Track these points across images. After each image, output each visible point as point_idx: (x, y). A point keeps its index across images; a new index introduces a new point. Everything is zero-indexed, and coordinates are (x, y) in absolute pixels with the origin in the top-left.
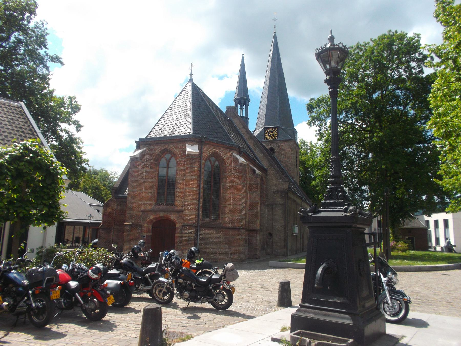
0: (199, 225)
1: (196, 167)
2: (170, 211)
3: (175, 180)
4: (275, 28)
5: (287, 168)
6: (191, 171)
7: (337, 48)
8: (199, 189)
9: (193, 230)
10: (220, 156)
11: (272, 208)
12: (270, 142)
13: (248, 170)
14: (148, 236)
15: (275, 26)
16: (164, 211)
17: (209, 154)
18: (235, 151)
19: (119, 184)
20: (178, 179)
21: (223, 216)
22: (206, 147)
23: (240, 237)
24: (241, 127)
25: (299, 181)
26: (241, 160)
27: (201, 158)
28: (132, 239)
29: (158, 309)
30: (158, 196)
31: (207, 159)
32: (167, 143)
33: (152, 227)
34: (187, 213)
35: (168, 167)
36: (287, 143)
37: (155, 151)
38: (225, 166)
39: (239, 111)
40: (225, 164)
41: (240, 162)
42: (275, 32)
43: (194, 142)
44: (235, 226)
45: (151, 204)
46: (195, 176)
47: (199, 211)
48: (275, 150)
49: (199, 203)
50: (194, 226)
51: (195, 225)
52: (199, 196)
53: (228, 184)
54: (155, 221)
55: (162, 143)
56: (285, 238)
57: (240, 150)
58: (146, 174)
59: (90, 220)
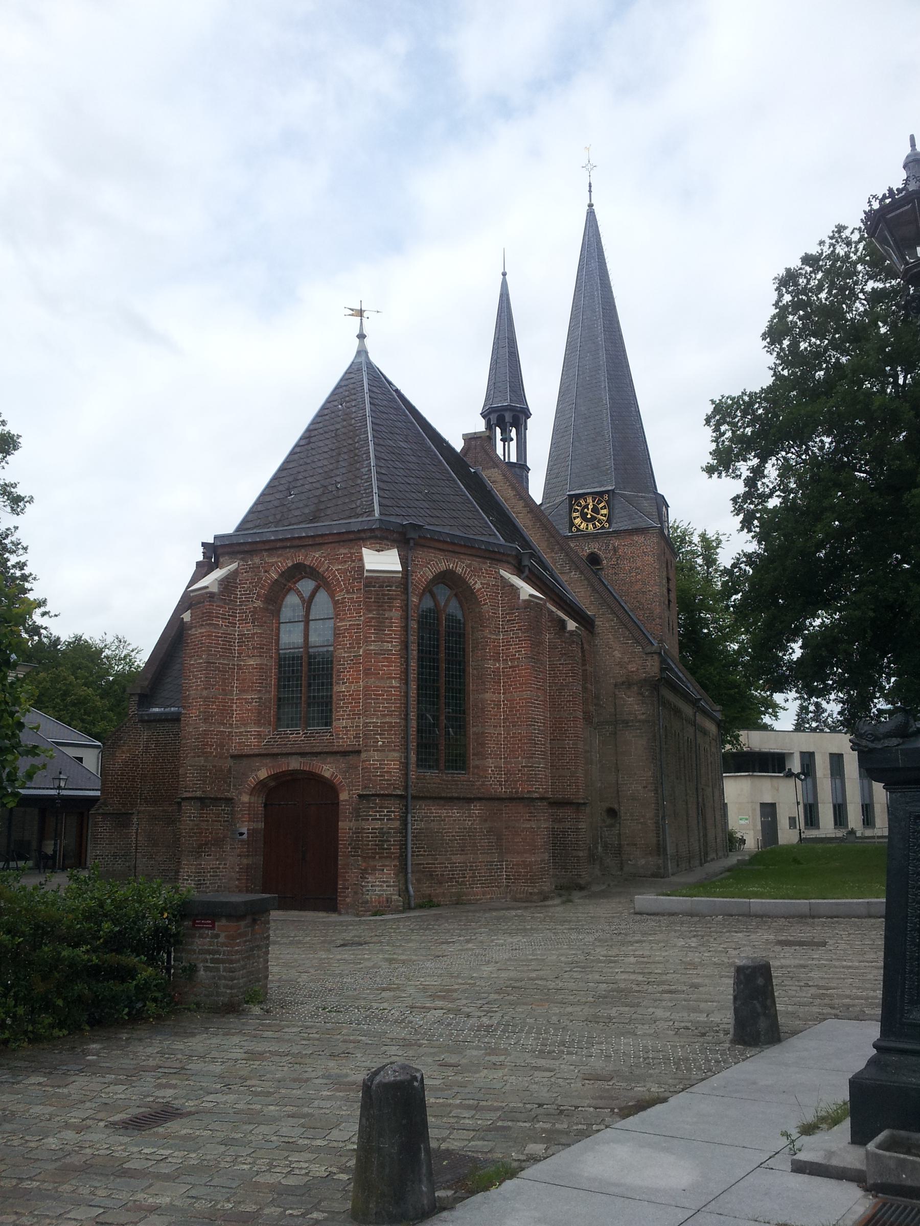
1: (395, 615)
2: (320, 753)
3: (332, 656)
4: (590, 191)
5: (641, 613)
6: (380, 629)
8: (407, 684)
9: (395, 809)
12: (587, 536)
14: (251, 833)
15: (590, 186)
16: (303, 754)
19: (150, 676)
21: (477, 763)
22: (421, 555)
24: (511, 493)
25: (677, 650)
26: (527, 590)
27: (406, 589)
28: (206, 844)
29: (416, 1084)
30: (279, 707)
31: (424, 591)
33: (266, 805)
34: (373, 758)
35: (307, 621)
37: (266, 572)
38: (477, 610)
39: (499, 445)
41: (524, 596)
43: (385, 542)
44: (517, 792)
45: (259, 735)
47: (407, 749)
49: (406, 726)
50: (397, 796)
52: (407, 707)
53: (490, 665)
54: (273, 784)
56: (657, 823)
57: (520, 562)
59: (59, 788)
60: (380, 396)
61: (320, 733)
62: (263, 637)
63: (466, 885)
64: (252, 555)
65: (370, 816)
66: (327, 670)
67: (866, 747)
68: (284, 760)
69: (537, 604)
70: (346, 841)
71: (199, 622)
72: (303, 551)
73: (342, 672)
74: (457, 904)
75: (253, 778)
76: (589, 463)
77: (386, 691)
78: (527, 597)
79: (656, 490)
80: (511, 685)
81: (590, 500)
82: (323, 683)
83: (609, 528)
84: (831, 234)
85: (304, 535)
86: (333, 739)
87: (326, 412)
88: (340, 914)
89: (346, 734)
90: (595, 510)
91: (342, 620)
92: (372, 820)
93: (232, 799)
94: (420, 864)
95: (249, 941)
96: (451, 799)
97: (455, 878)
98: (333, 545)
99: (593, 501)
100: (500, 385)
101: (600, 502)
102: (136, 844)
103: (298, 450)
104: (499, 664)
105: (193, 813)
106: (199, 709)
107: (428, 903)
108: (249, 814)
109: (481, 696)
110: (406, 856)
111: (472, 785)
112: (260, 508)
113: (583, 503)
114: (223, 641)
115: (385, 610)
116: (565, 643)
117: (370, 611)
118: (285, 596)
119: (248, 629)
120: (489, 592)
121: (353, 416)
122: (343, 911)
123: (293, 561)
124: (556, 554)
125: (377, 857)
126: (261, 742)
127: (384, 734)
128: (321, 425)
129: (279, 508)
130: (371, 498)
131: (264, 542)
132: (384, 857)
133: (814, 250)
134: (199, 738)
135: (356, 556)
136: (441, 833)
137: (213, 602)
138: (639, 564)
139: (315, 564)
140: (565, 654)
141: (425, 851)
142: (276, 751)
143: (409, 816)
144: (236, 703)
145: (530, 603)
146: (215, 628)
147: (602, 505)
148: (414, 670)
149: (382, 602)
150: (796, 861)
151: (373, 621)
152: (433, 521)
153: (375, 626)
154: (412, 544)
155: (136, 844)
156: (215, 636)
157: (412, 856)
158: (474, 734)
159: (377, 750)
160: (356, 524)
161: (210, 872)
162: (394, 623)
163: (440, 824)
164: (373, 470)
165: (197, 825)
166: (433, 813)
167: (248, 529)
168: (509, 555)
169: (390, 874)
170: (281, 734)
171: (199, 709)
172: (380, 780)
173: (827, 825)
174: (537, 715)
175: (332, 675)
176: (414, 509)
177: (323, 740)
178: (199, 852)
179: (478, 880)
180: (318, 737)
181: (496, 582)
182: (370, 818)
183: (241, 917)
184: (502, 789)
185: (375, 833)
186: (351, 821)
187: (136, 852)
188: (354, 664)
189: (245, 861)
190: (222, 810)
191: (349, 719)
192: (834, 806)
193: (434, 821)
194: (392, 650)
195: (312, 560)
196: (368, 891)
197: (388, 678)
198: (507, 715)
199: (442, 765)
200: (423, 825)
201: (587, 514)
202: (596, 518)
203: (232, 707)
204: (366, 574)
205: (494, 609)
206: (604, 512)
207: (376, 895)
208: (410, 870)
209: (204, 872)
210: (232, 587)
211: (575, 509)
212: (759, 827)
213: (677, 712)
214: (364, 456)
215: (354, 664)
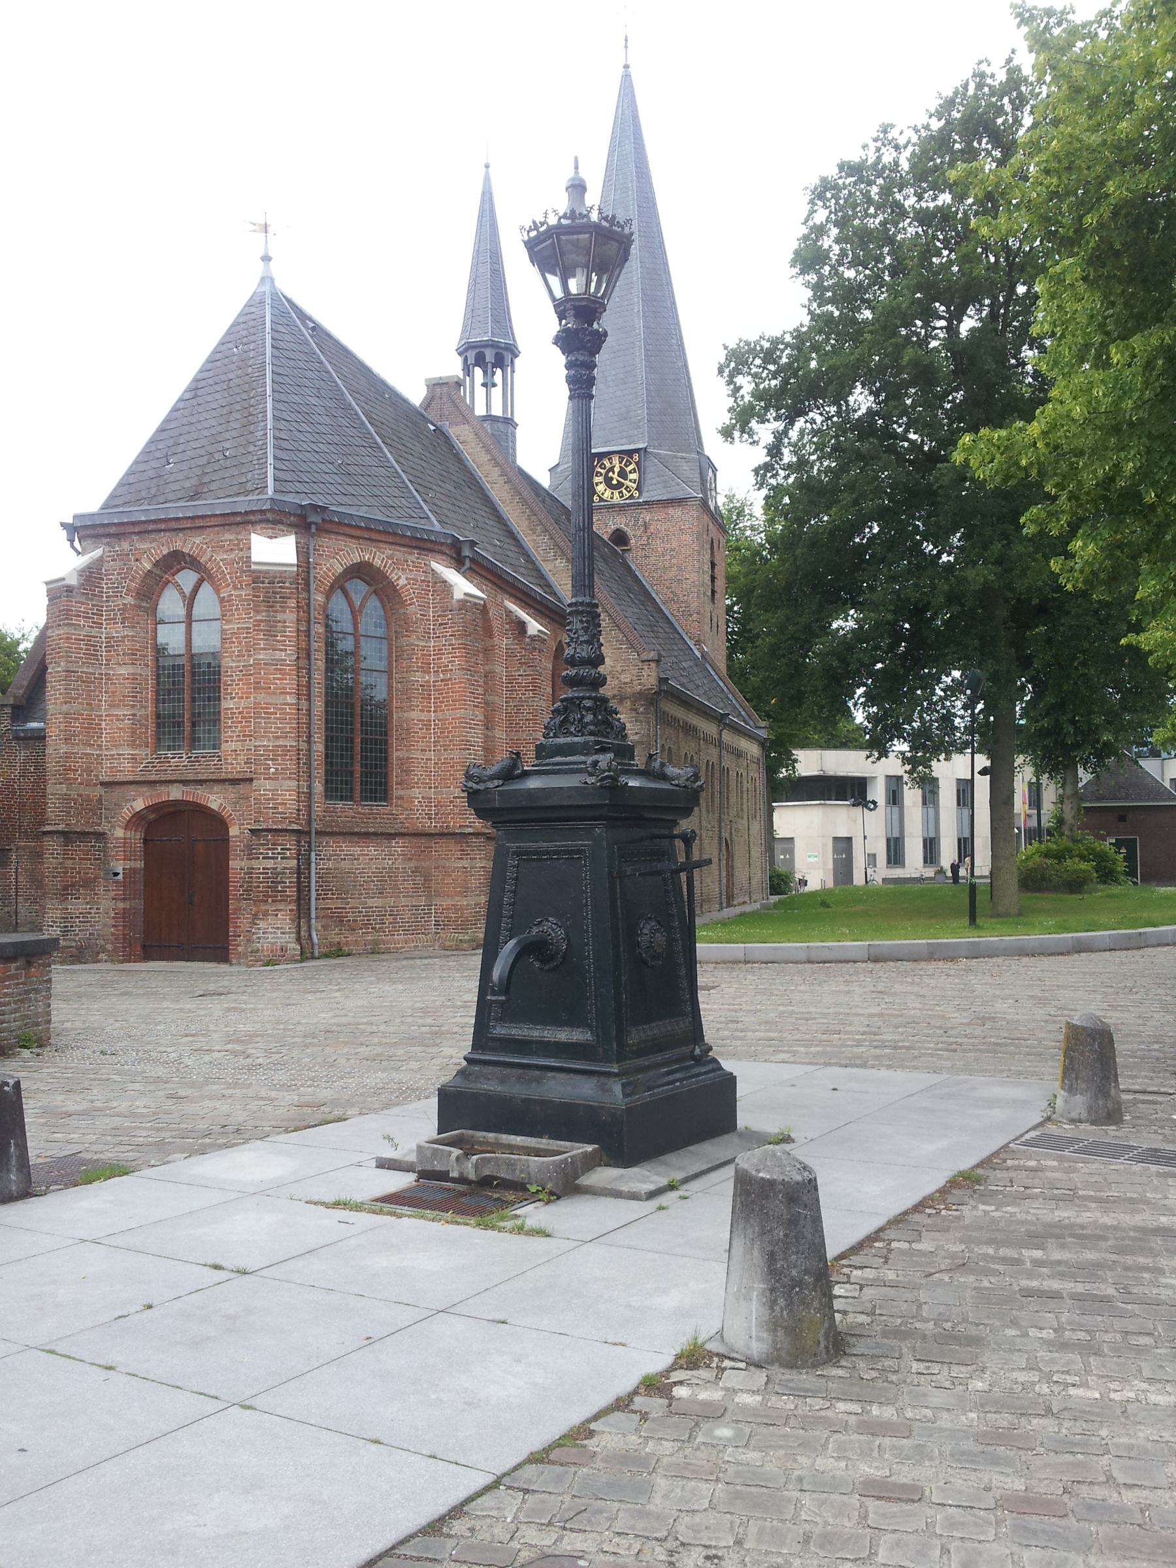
0: (314, 826)
2: (205, 781)
6: (270, 633)
7: (546, 231)
14: (129, 873)
17: (340, 570)
18: (439, 556)
20: (227, 662)
21: (401, 793)
22: (328, 543)
23: (465, 863)
24: (485, 457)
25: (724, 652)
26: (462, 586)
27: (308, 585)
28: (73, 885)
31: (332, 586)
33: (145, 841)
34: (263, 786)
35: (189, 621)
36: (675, 512)
37: (137, 560)
38: (402, 611)
39: (480, 392)
40: (403, 603)
41: (458, 595)
43: (280, 526)
46: (287, 655)
48: (633, 541)
50: (293, 831)
51: (295, 827)
54: (152, 817)
57: (459, 552)
58: (109, 647)
60: (288, 337)
62: (136, 641)
63: (384, 932)
65: (261, 853)
66: (215, 683)
67: (471, 788)
68: (163, 788)
69: (475, 604)
70: (237, 882)
71: (55, 621)
72: (181, 535)
74: (373, 953)
76: (616, 412)
77: (280, 709)
78: (462, 597)
79: (703, 449)
80: (443, 702)
81: (616, 460)
82: (209, 698)
83: (638, 498)
84: (875, 135)
85: (181, 515)
87: (218, 356)
88: (231, 964)
89: (235, 759)
90: (623, 474)
91: (229, 622)
92: (263, 858)
93: (104, 834)
94: (329, 909)
95: (22, 984)
96: (367, 835)
97: (371, 924)
98: (216, 529)
99: (620, 463)
100: (479, 312)
101: (628, 464)
102: (17, 885)
103: (181, 405)
104: (430, 677)
105: (56, 850)
106: (59, 727)
107: (337, 952)
108: (124, 851)
110: (309, 899)
111: (395, 819)
112: (132, 479)
113: (608, 465)
114: (86, 645)
115: (276, 611)
116: (525, 649)
117: (258, 612)
119: (118, 631)
121: (250, 363)
122: (234, 961)
123: (169, 548)
124: (538, 536)
126: (137, 767)
127: (277, 760)
128: (211, 374)
129: (155, 481)
130: (264, 470)
131: (133, 524)
132: (277, 901)
133: (855, 156)
134: (59, 762)
135: (244, 544)
136: (355, 873)
138: (675, 544)
139: (195, 552)
140: (525, 663)
141: (333, 894)
142: (153, 778)
143: (313, 854)
145: (466, 604)
146: (75, 629)
148: (319, 683)
150: (824, 904)
151: (262, 624)
152: (345, 500)
154: (313, 530)
155: (17, 885)
158: (398, 759)
159: (269, 778)
160: (242, 504)
161: (79, 917)
163: (353, 864)
164: (270, 435)
165: (60, 864)
167: (116, 506)
168: (442, 544)
169: (285, 920)
171: (59, 727)
173: (914, 862)
174: (473, 737)
175: (220, 687)
176: (321, 485)
178: (64, 895)
179: (400, 927)
181: (426, 577)
182: (261, 856)
183: (13, 959)
184: (431, 823)
186: (242, 860)
187: (16, 895)
188: (243, 675)
189: (121, 905)
190: (92, 846)
192: (925, 841)
194: (285, 660)
195: (192, 548)
196: (259, 938)
197: (282, 693)
198: (439, 737)
199: (357, 795)
200: (330, 864)
201: (612, 479)
202: (623, 485)
203: (100, 725)
204: (253, 567)
205: (424, 610)
206: (634, 476)
207: (269, 943)
208: (313, 915)
209: (71, 918)
210: (95, 578)
211: (598, 472)
212: (830, 866)
213: (690, 730)
214: (261, 415)
215: (243, 675)
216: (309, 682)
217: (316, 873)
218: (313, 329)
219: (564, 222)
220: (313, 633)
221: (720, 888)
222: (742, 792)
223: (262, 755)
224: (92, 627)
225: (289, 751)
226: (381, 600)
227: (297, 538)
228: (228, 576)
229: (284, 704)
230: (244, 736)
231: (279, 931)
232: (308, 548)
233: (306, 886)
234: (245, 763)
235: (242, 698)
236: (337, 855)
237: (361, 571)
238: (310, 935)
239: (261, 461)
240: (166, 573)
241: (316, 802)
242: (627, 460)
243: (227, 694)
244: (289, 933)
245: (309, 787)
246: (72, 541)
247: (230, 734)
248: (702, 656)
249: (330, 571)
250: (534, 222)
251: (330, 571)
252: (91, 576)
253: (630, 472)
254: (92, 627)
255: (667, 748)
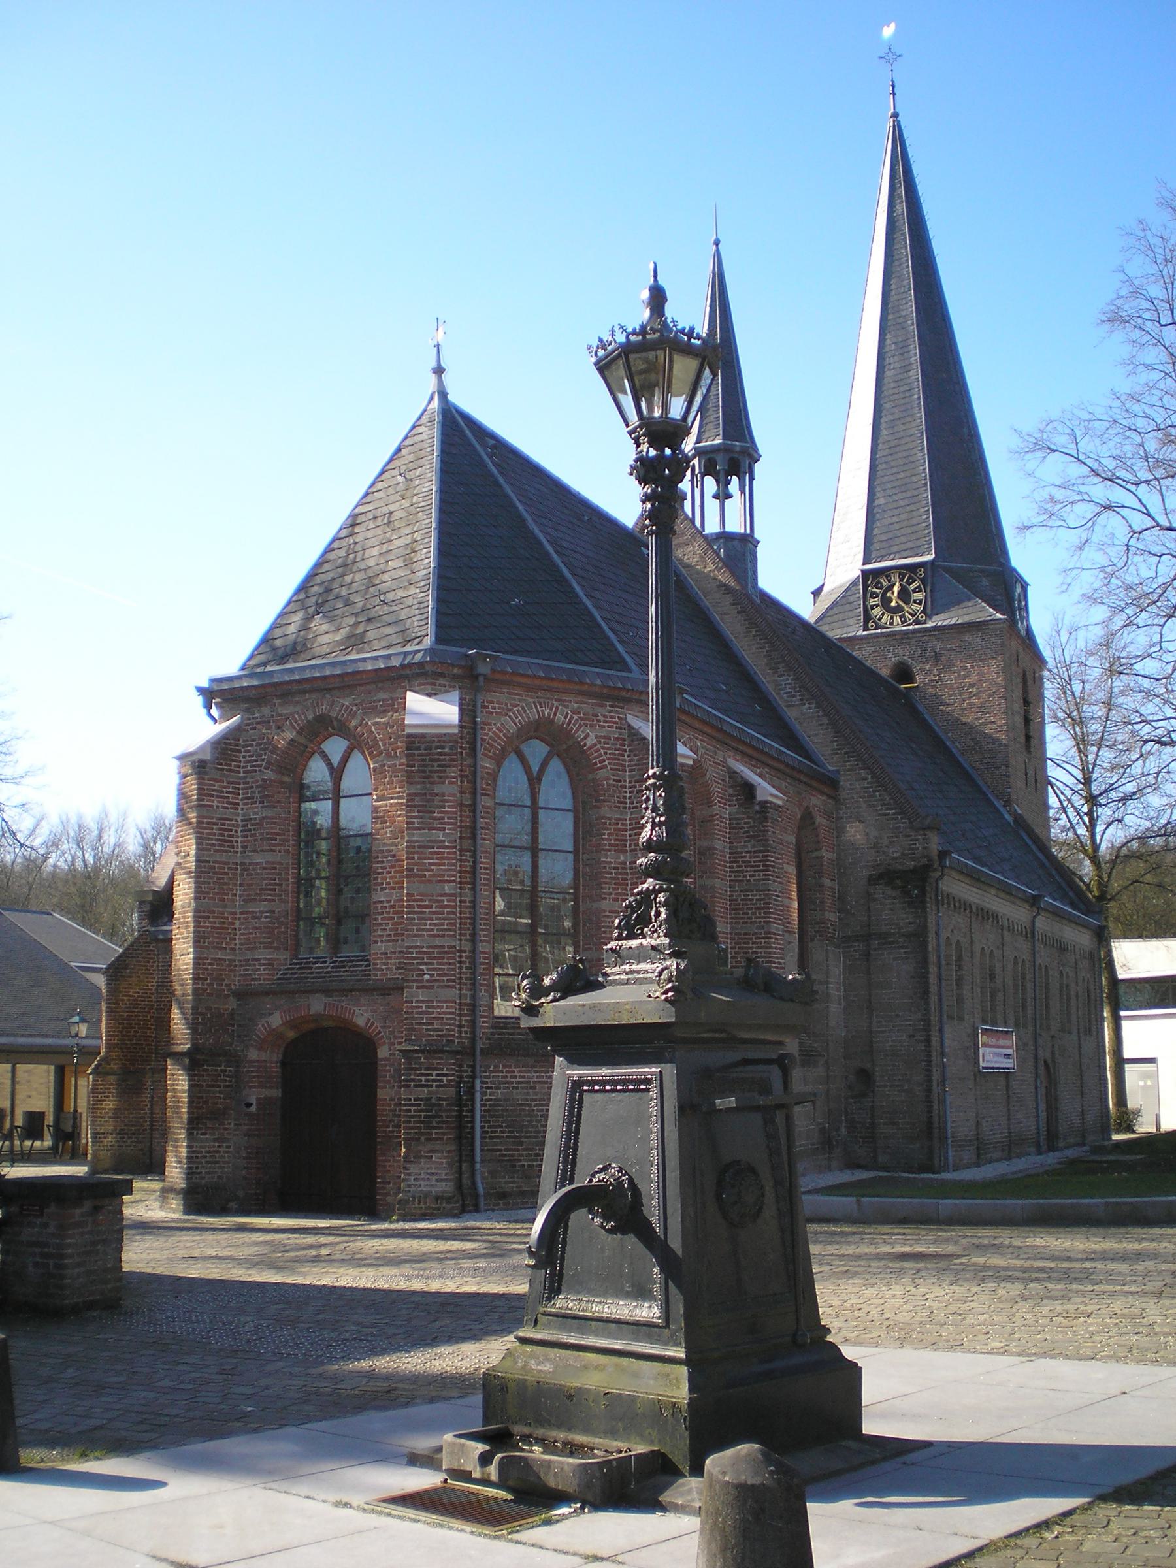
0: (479, 1045)
10: (569, 735)
11: (867, 955)
13: (716, 788)
14: (263, 1103)
16: (327, 992)
22: (495, 699)
32: (329, 690)
33: (283, 1064)
34: (416, 997)
35: (337, 796)
38: (590, 777)
39: (712, 505)
40: (592, 768)
42: (895, 115)
43: (441, 681)
54: (291, 1035)
55: (304, 692)
61: (353, 961)
62: (275, 823)
64: (259, 705)
65: (413, 1080)
73: (379, 873)
75: (263, 1026)
81: (896, 578)
86: (370, 970)
89: (384, 964)
92: (416, 1086)
99: (901, 580)
102: (152, 1118)
109: (595, 905)
113: (885, 583)
114: (220, 829)
118: (307, 762)
120: (608, 749)
121: (415, 492)
123: (314, 712)
125: (423, 1138)
127: (433, 964)
135: (399, 703)
136: (530, 1105)
137: (205, 773)
144: (239, 918)
147: (913, 586)
148: (486, 869)
149: (430, 771)
151: (417, 799)
153: (419, 806)
156: (208, 823)
157: (482, 1138)
161: (206, 1157)
162: (447, 801)
166: (516, 1077)
170: (301, 963)
172: (428, 1030)
177: (356, 971)
180: (350, 966)
185: (420, 1105)
190: (221, 1070)
191: (389, 941)
193: (517, 1088)
194: (444, 841)
195: (340, 711)
196: (409, 1186)
197: (440, 882)
203: (234, 924)
204: (408, 731)
205: (618, 775)
208: (478, 1158)
209: (197, 1157)
210: (232, 750)
211: (873, 593)
216: (474, 867)
217: (482, 1105)
218: (494, 447)
219: (633, 338)
220: (479, 807)
221: (1038, 1124)
222: (1069, 999)
223: (414, 958)
224: (226, 808)
225: (446, 952)
226: (565, 764)
227: (461, 693)
228: (380, 743)
229: (441, 895)
230: (395, 935)
231: (434, 1178)
232: (474, 706)
233: (468, 1122)
234: (397, 968)
235: (394, 888)
236: (507, 1082)
237: (540, 729)
238: (474, 1183)
239: (422, 605)
240: (311, 741)
241: (482, 1016)
242: (910, 577)
243: (377, 884)
244: (446, 1180)
245: (473, 997)
246: (208, 707)
247: (379, 933)
248: (1015, 821)
249: (501, 731)
250: (601, 340)
251: (501, 731)
252: (224, 746)
253: (914, 591)
254: (226, 808)
255: (954, 942)
